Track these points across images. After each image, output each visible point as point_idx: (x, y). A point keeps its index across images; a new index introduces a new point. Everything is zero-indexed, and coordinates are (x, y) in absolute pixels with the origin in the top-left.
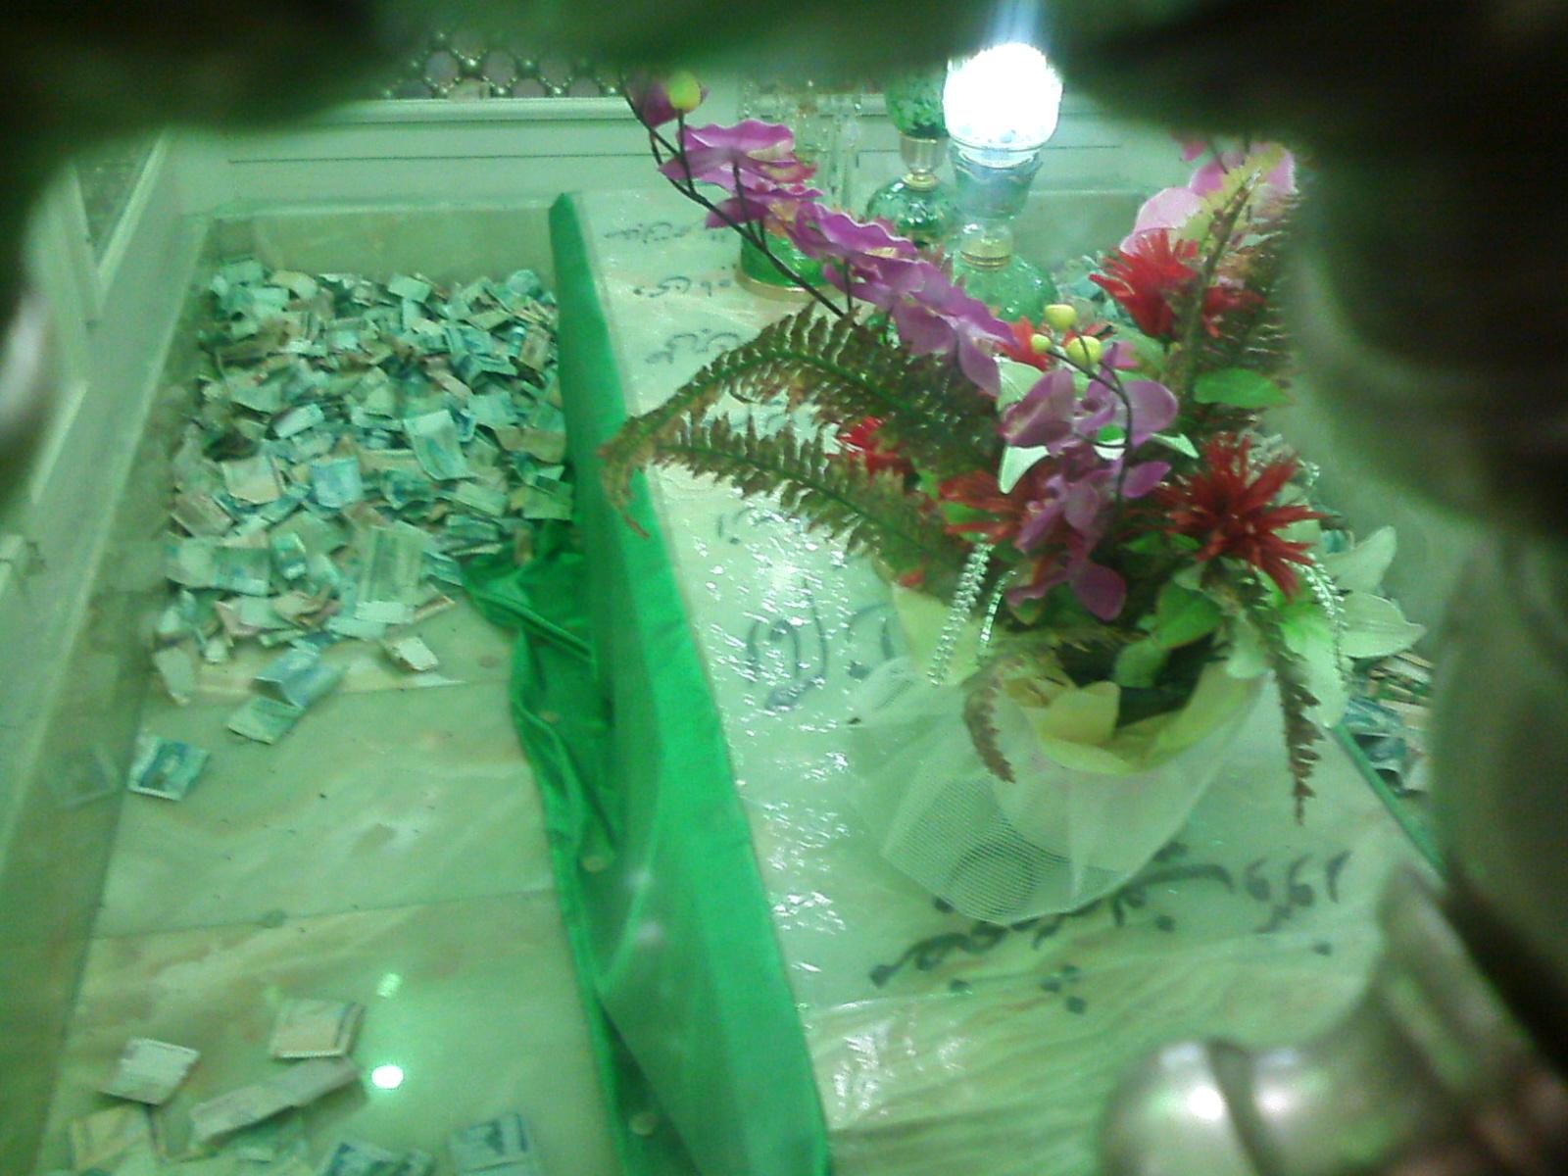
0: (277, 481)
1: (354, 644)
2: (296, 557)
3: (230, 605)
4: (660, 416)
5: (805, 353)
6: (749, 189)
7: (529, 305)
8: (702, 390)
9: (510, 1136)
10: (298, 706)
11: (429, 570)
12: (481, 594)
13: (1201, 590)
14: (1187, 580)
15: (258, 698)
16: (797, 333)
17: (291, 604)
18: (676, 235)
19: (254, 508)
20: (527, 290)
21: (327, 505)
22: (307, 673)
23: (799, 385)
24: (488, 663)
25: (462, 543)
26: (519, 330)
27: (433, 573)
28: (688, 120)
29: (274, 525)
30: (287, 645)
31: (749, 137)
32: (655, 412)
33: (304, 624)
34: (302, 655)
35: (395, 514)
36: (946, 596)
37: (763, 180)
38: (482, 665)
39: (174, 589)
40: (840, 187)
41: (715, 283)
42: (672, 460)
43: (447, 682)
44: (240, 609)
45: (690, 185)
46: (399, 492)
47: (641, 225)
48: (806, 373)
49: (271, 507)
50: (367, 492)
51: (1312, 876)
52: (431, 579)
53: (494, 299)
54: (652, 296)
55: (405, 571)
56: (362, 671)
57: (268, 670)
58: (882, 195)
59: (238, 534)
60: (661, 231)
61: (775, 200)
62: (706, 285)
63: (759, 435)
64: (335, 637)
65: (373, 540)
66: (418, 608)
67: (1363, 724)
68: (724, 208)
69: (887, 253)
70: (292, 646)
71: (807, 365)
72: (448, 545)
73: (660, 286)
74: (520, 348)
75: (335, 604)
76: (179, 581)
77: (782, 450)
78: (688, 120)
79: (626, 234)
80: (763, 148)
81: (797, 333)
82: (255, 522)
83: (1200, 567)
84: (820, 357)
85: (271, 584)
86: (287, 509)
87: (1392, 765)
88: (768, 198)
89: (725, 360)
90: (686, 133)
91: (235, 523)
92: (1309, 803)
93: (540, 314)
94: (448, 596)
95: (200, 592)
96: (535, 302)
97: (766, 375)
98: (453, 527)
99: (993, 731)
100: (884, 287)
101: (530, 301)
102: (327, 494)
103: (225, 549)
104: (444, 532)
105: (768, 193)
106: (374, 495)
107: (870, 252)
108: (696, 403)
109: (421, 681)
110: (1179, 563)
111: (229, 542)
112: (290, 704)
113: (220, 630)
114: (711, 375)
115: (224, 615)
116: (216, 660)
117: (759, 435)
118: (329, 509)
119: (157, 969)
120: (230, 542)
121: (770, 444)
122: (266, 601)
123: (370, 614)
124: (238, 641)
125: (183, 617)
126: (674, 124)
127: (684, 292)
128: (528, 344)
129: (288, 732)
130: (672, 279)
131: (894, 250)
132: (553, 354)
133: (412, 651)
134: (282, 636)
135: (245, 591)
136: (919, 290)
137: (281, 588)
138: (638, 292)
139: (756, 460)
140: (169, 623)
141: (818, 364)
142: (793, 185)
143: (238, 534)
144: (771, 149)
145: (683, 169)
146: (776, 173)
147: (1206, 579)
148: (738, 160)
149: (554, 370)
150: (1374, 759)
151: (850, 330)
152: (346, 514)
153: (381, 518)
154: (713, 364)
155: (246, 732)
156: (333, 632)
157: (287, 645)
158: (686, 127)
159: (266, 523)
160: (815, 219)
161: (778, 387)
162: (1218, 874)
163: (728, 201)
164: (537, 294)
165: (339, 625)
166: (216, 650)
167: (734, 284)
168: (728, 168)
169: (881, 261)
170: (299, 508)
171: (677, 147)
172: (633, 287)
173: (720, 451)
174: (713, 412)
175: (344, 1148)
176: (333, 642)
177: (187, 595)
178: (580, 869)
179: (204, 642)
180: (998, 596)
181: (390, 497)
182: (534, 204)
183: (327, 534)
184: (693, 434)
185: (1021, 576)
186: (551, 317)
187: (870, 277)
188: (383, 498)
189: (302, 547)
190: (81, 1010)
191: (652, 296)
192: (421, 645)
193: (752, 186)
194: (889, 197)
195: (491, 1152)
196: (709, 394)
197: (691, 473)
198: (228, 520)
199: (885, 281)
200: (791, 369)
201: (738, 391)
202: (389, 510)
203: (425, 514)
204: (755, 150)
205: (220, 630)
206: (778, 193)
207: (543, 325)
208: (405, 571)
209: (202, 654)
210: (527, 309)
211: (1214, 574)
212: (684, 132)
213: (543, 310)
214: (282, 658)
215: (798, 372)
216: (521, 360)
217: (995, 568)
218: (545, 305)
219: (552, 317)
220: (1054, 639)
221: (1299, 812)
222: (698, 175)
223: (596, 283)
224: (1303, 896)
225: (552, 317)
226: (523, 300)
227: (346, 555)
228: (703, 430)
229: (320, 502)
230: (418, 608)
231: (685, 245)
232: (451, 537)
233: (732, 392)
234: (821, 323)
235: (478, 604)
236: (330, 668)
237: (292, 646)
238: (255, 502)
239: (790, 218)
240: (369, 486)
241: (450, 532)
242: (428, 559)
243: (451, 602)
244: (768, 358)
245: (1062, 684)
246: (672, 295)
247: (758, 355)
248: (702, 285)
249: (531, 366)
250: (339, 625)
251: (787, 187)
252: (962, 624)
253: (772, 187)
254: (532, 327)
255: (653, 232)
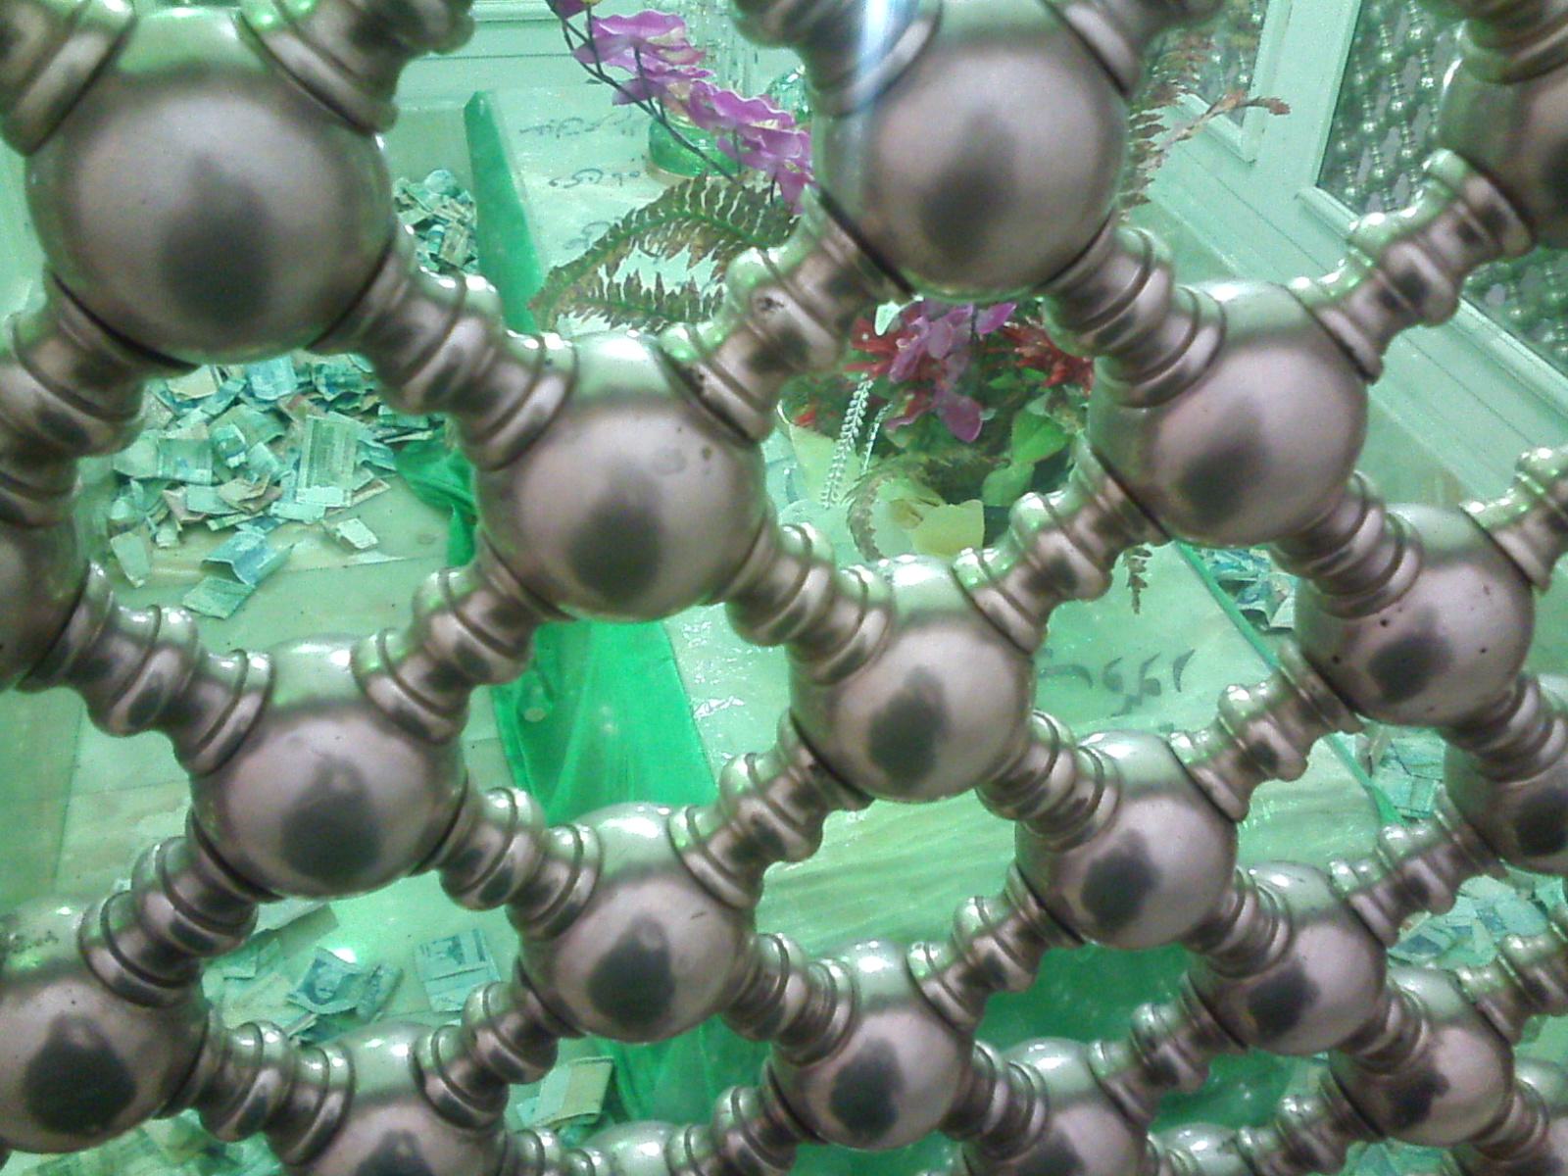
0: (214, 376)
1: (297, 528)
2: (236, 446)
3: (179, 493)
4: (579, 268)
5: (703, 214)
6: (649, 71)
7: (447, 204)
8: (615, 245)
9: (468, 947)
10: (249, 584)
11: (364, 456)
12: (418, 478)
13: (1048, 415)
14: (1037, 408)
15: (209, 579)
16: (695, 195)
17: (235, 490)
18: (588, 130)
19: (195, 403)
20: (443, 189)
21: (265, 398)
22: (253, 554)
23: (698, 242)
24: (425, 540)
25: (394, 431)
26: (437, 228)
27: (368, 459)
28: (595, 12)
29: (214, 417)
30: (234, 529)
31: (650, 26)
32: (576, 262)
33: (249, 509)
34: (249, 537)
35: (329, 406)
36: (833, 433)
37: (660, 63)
38: (420, 542)
39: (122, 481)
40: (741, 82)
41: (625, 174)
42: (592, 313)
43: (387, 559)
44: (186, 495)
45: (599, 67)
46: (331, 385)
47: (552, 121)
48: (704, 231)
49: (212, 400)
50: (301, 385)
51: (1161, 672)
52: (365, 464)
53: (413, 199)
54: (566, 187)
55: (342, 458)
56: (306, 550)
57: (219, 552)
58: (778, 85)
59: (179, 427)
60: (573, 126)
61: (673, 80)
62: (618, 176)
63: (667, 291)
64: (280, 521)
65: (310, 427)
66: (356, 493)
67: (1236, 571)
68: (628, 87)
69: (771, 125)
70: (238, 530)
71: (705, 225)
72: (380, 434)
73: (573, 178)
74: (441, 246)
75: (278, 491)
76: (128, 473)
77: (687, 303)
78: (595, 12)
79: (540, 130)
80: (660, 34)
81: (695, 195)
82: (196, 415)
83: (1048, 393)
84: (715, 217)
85: (214, 474)
86: (222, 405)
87: (1260, 605)
88: (665, 77)
89: (634, 217)
90: (593, 22)
91: (177, 418)
92: (1143, 593)
93: (458, 212)
94: (384, 480)
95: (145, 482)
96: (453, 200)
97: (669, 234)
98: (384, 416)
99: (871, 531)
100: (769, 156)
101: (447, 200)
102: (263, 388)
103: (168, 440)
104: (375, 422)
105: (665, 73)
106: (308, 388)
107: (754, 124)
108: (610, 258)
109: (363, 558)
110: (1031, 394)
111: (171, 435)
112: (238, 581)
113: (169, 517)
114: (622, 232)
115: (171, 501)
116: (167, 545)
117: (667, 291)
118: (266, 402)
119: (136, 818)
120: (171, 435)
121: (677, 297)
122: (210, 489)
123: (308, 499)
124: (185, 525)
125: (133, 506)
126: (584, 15)
127: (597, 183)
128: (447, 242)
129: (240, 607)
130: (586, 170)
131: (776, 122)
132: (475, 251)
133: (353, 530)
134: (229, 521)
135: (191, 480)
136: (797, 157)
137: (225, 476)
138: (553, 184)
139: (666, 312)
140: (120, 511)
141: (714, 224)
142: (687, 67)
143: (179, 427)
144: (666, 35)
145: (594, 50)
146: (672, 56)
147: (1051, 406)
148: (639, 46)
149: (474, 267)
150: (1243, 600)
151: (740, 194)
152: (282, 406)
153: (315, 408)
154: (623, 221)
155: (203, 609)
156: (276, 516)
157: (234, 529)
158: (595, 18)
159: (206, 416)
160: (707, 96)
161: (682, 245)
162: (1083, 673)
163: (631, 80)
164: (455, 193)
165: (282, 509)
166: (166, 536)
167: (644, 175)
168: (630, 53)
169: (764, 131)
170: (237, 402)
171: (586, 36)
172: (547, 180)
173: (633, 304)
174: (626, 268)
175: (318, 964)
176: (277, 526)
177: (134, 484)
178: (522, 720)
179: (154, 527)
180: (877, 426)
181: (323, 389)
182: (448, 105)
183: (263, 425)
184: (609, 288)
185: (895, 410)
186: (469, 215)
187: (757, 146)
188: (316, 391)
189: (242, 437)
190: (67, 857)
191: (566, 187)
192: (361, 525)
193: (652, 67)
194: (784, 87)
195: (452, 961)
196: (621, 250)
197: (609, 324)
198: (169, 415)
199: (769, 150)
200: (692, 228)
201: (646, 247)
202: (322, 401)
203: (358, 404)
204: (653, 37)
205: (169, 517)
206: (673, 73)
207: (461, 222)
208: (342, 458)
209: (154, 539)
210: (445, 207)
211: (1059, 400)
212: (592, 21)
213: (462, 209)
214: (231, 541)
215: (697, 230)
216: (441, 256)
217: (874, 404)
218: (462, 203)
219: (470, 215)
220: (923, 458)
221: (1137, 603)
222: (605, 60)
223: (514, 176)
224: (1154, 688)
225: (470, 215)
226: (441, 199)
227: (285, 445)
228: (618, 285)
229: (257, 395)
230: (356, 493)
231: (598, 138)
232: (383, 426)
233: (641, 247)
234: (715, 190)
235: (413, 487)
236: (277, 548)
237: (238, 530)
238: (196, 396)
239: (685, 96)
240: (302, 379)
241: (382, 421)
242: (362, 446)
243: (387, 486)
244: (670, 217)
245: (935, 505)
246: (586, 186)
247: (662, 214)
248: (614, 175)
249: (451, 262)
250: (282, 509)
251: (683, 69)
252: (847, 453)
253: (668, 68)
254: (450, 225)
255: (566, 127)
